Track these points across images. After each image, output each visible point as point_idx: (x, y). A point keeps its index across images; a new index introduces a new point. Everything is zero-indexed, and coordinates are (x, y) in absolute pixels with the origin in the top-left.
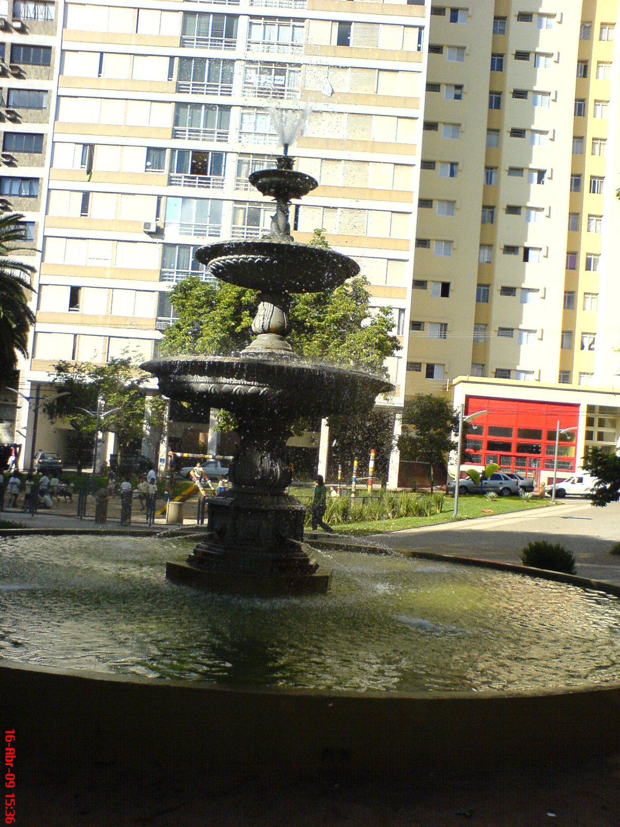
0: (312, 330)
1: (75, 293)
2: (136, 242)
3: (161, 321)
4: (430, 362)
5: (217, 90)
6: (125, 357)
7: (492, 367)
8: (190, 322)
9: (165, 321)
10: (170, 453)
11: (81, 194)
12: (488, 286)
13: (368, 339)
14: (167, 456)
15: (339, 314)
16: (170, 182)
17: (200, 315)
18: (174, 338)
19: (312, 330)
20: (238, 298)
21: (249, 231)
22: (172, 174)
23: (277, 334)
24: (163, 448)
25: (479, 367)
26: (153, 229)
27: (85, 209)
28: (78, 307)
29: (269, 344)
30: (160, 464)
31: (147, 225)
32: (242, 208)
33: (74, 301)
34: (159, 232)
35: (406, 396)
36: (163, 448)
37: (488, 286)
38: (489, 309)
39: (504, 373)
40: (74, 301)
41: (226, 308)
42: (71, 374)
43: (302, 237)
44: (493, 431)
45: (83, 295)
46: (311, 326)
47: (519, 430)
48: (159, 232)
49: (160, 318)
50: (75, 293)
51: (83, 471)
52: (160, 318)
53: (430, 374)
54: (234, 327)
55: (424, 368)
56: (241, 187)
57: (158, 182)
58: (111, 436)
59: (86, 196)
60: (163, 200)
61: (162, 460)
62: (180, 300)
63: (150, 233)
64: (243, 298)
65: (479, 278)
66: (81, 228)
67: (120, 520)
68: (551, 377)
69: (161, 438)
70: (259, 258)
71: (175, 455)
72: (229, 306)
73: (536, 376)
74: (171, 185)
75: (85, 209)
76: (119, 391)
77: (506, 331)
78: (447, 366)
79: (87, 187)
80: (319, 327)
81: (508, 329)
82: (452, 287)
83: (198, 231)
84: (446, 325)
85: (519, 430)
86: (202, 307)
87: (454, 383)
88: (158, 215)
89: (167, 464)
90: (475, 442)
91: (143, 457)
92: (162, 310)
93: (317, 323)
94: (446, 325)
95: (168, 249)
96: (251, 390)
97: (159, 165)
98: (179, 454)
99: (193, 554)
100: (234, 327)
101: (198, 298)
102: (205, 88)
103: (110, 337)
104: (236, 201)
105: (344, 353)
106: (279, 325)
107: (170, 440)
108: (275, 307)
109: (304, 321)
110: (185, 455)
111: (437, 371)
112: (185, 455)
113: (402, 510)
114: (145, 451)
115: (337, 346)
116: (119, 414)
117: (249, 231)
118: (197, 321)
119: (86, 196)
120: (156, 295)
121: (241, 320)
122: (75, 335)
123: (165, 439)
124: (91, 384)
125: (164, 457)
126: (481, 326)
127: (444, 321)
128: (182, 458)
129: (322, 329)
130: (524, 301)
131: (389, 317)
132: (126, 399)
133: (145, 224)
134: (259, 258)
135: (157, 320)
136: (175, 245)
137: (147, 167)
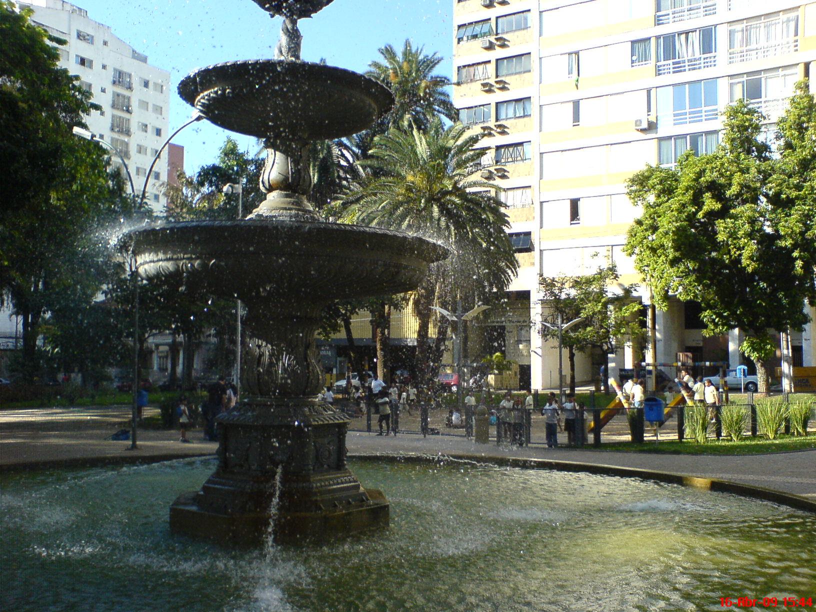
2: (630, 142)
5: (701, 116)
11: (571, 104)
16: (658, 72)
20: (696, 180)
22: (659, 64)
23: (281, 190)
26: (645, 125)
27: (576, 118)
28: (579, 220)
31: (638, 122)
32: (739, 83)
33: (575, 214)
34: (652, 127)
40: (575, 214)
41: (684, 194)
43: (309, 55)
45: (581, 205)
48: (652, 127)
50: (574, 205)
51: (593, 388)
54: (695, 214)
56: (737, 59)
57: (645, 74)
59: (576, 104)
60: (653, 92)
63: (643, 130)
64: (702, 179)
66: (576, 137)
67: (496, 439)
72: (687, 191)
74: (659, 74)
75: (576, 118)
79: (576, 97)
83: (692, 118)
88: (649, 110)
95: (664, 143)
97: (645, 57)
99: (202, 493)
100: (695, 214)
102: (688, 116)
103: (612, 246)
104: (731, 76)
106: (280, 178)
108: (277, 152)
119: (576, 104)
121: (703, 203)
133: (636, 121)
136: (670, 138)
137: (633, 62)
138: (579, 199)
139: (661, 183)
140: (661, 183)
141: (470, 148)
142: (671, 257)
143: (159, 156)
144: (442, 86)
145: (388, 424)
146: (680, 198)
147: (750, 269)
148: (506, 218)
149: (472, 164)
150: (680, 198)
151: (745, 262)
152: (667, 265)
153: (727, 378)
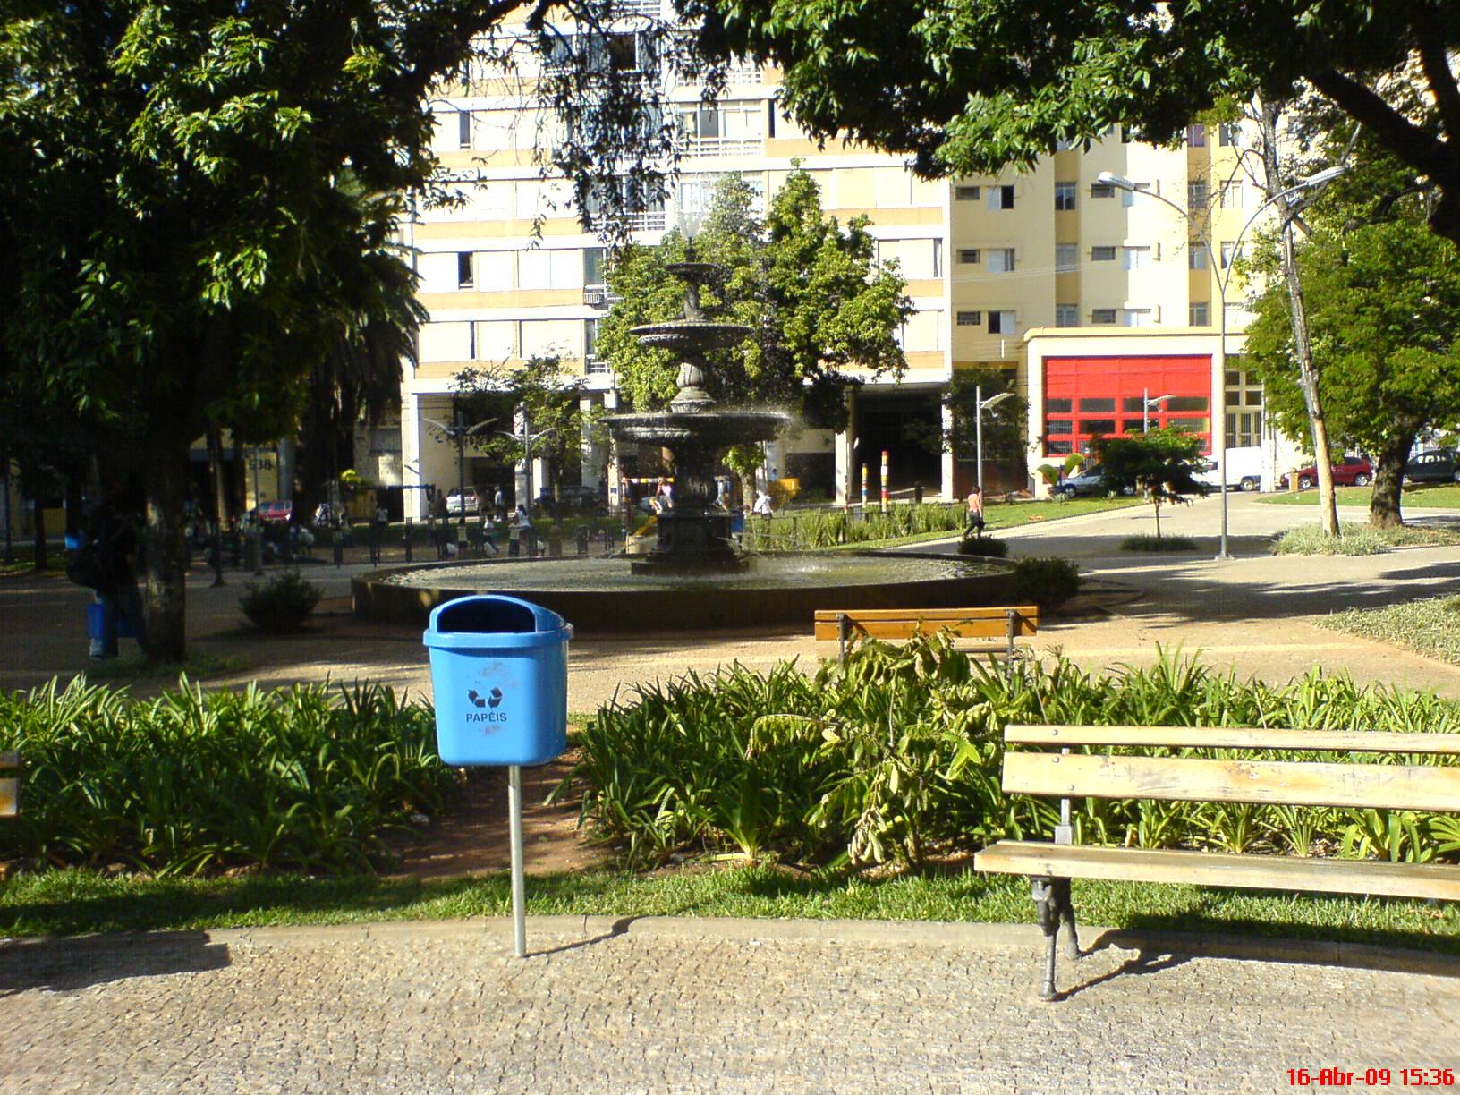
0: (794, 301)
1: (465, 260)
3: (590, 291)
4: (994, 308)
6: (552, 356)
7: (1086, 310)
8: (631, 306)
9: (597, 290)
10: (624, 480)
12: (1074, 184)
13: (866, 309)
14: (620, 484)
15: (830, 276)
17: (645, 295)
18: (613, 329)
19: (794, 301)
21: (705, 146)
24: (613, 474)
25: (1067, 315)
29: (690, 395)
30: (610, 495)
33: (465, 273)
35: (954, 364)
36: (613, 474)
37: (1074, 184)
38: (1077, 220)
39: (1106, 316)
40: (465, 273)
42: (480, 383)
44: (1088, 404)
45: (475, 262)
46: (792, 296)
47: (1125, 400)
49: (588, 287)
50: (465, 260)
52: (588, 287)
53: (995, 326)
55: (985, 319)
58: (538, 465)
61: (613, 490)
62: (617, 278)
65: (1057, 174)
68: (1178, 317)
69: (608, 461)
70: (675, 336)
71: (630, 483)
73: (1154, 315)
76: (548, 404)
77: (1104, 253)
78: (1019, 314)
80: (802, 296)
81: (1108, 248)
82: (1016, 192)
84: (1013, 251)
85: (1125, 400)
86: (646, 284)
87: (1026, 338)
89: (621, 496)
90: (1061, 422)
91: (586, 488)
92: (590, 274)
93: (799, 292)
94: (1013, 251)
96: (677, 434)
98: (635, 481)
101: (640, 274)
105: (838, 329)
107: (622, 460)
109: (784, 289)
110: (643, 480)
111: (1004, 322)
112: (643, 480)
113: (921, 526)
114: (588, 479)
115: (828, 320)
116: (551, 435)
117: (705, 146)
118: (641, 303)
120: (581, 252)
122: (472, 323)
123: (615, 461)
124: (508, 394)
125: (616, 486)
126: (1066, 249)
127: (1009, 245)
128: (639, 484)
129: (807, 298)
130: (1127, 203)
131: (896, 272)
132: (558, 413)
134: (675, 336)
135: (585, 290)
138: (470, 254)
139: (649, 269)
140: (649, 269)
141: (891, 744)
142: (666, 358)
143: (543, 180)
144: (1066, 920)
145: (109, 696)
146: (672, 289)
147: (753, 375)
148: (405, 362)
149: (462, 937)
150: (672, 289)
151: (747, 366)
152: (660, 368)
153: (1017, 640)
